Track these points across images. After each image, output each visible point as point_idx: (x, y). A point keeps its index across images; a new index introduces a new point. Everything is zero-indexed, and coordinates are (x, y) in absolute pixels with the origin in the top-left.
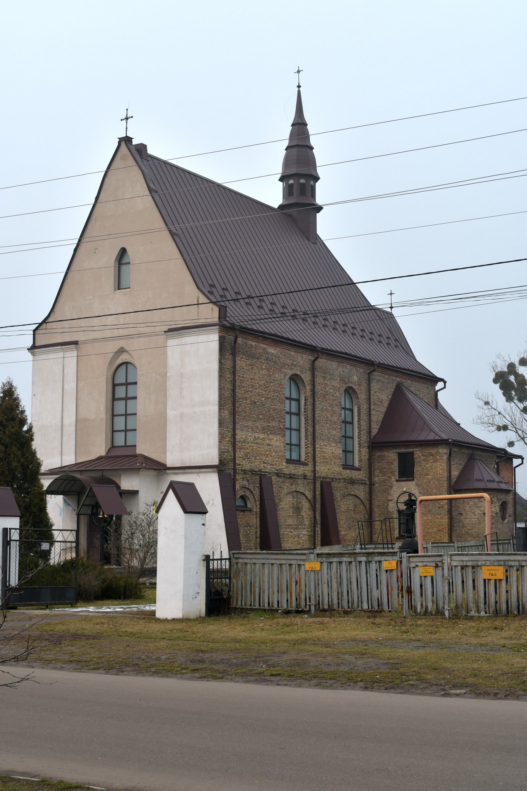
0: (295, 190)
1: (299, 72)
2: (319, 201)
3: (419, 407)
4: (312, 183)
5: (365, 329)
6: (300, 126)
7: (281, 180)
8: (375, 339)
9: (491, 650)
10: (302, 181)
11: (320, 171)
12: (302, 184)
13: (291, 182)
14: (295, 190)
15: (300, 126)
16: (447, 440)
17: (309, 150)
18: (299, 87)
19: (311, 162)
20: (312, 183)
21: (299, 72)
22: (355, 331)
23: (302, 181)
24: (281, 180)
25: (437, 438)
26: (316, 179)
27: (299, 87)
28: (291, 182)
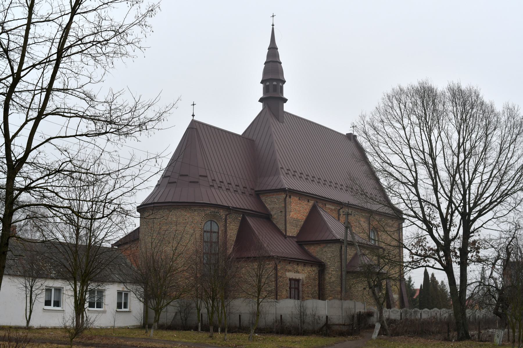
0: (271, 89)
1: (273, 16)
2: (285, 95)
3: (326, 219)
4: (281, 84)
5: (303, 172)
6: (273, 50)
7: (262, 82)
8: (327, 184)
9: (22, 106)
10: (275, 83)
11: (286, 77)
12: (274, 85)
13: (268, 84)
14: (271, 89)
15: (273, 50)
16: (339, 240)
17: (278, 64)
18: (273, 25)
19: (280, 71)
20: (281, 84)
21: (273, 16)
22: (332, 184)
23: (275, 83)
24: (262, 82)
25: (334, 238)
26: (284, 82)
27: (273, 25)
28: (268, 84)
